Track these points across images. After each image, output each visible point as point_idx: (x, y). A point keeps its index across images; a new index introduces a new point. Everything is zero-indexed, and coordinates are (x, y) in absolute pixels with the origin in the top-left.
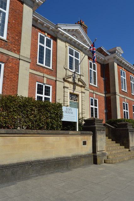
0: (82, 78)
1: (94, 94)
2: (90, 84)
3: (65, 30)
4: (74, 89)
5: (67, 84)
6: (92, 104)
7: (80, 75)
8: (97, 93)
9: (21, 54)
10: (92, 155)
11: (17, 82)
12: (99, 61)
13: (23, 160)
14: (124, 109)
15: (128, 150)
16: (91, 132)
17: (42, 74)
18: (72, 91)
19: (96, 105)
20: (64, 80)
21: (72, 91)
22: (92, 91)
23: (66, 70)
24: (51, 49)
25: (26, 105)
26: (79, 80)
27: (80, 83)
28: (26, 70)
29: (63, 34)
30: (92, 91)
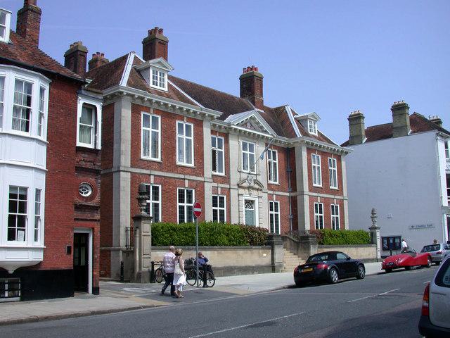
0: (259, 178)
5: (241, 191)
6: (271, 210)
7: (256, 175)
8: (277, 193)
12: (278, 144)
14: (333, 214)
17: (182, 176)
19: (276, 210)
20: (239, 186)
22: (271, 192)
27: (256, 186)
30: (271, 192)
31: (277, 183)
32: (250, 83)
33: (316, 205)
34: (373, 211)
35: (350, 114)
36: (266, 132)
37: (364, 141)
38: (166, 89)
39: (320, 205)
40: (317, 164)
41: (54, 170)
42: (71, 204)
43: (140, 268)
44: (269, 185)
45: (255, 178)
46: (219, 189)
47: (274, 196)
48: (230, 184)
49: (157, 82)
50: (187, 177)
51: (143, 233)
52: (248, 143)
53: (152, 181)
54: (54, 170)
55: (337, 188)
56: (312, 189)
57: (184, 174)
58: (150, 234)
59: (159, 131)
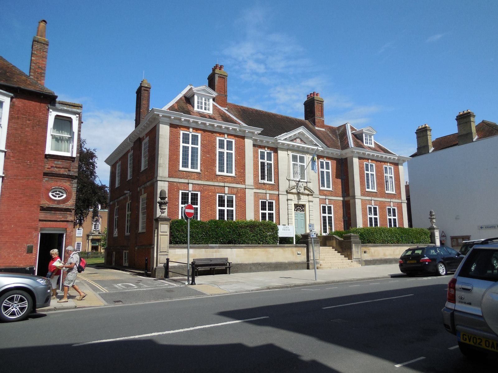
0: (310, 185)
1: (327, 200)
2: (321, 188)
3: (285, 139)
4: (299, 199)
5: (290, 196)
7: (307, 182)
9: (246, 183)
10: (307, 262)
11: (245, 207)
13: (255, 262)
15: (351, 261)
16: (305, 245)
17: (222, 184)
18: (296, 203)
19: (394, 215)
21: (297, 202)
22: (324, 197)
23: (289, 181)
24: (272, 162)
25: (252, 226)
26: (305, 188)
27: (307, 192)
28: (251, 196)
29: (283, 144)
30: (324, 197)
31: (331, 189)
32: (312, 107)
33: (370, 208)
34: (431, 212)
35: (417, 128)
36: (316, 145)
37: (430, 151)
38: (211, 112)
39: (375, 208)
40: (372, 172)
41: (17, 176)
42: (36, 206)
43: (157, 265)
44: (321, 192)
45: (305, 185)
46: (268, 195)
47: (327, 200)
48: (279, 191)
49: (367, 142)
50: (226, 184)
51: (160, 233)
52: (298, 155)
53: (190, 189)
54: (17, 176)
55: (394, 192)
56: (364, 193)
57: (224, 182)
58: (168, 233)
59: (199, 147)
